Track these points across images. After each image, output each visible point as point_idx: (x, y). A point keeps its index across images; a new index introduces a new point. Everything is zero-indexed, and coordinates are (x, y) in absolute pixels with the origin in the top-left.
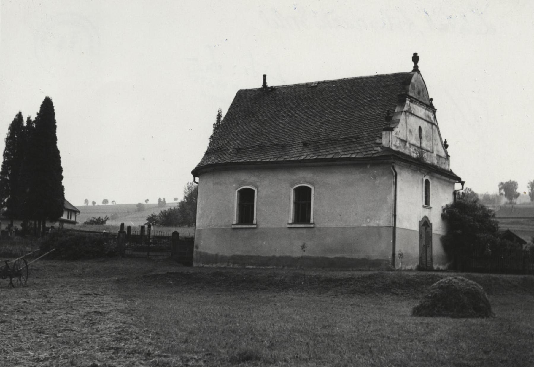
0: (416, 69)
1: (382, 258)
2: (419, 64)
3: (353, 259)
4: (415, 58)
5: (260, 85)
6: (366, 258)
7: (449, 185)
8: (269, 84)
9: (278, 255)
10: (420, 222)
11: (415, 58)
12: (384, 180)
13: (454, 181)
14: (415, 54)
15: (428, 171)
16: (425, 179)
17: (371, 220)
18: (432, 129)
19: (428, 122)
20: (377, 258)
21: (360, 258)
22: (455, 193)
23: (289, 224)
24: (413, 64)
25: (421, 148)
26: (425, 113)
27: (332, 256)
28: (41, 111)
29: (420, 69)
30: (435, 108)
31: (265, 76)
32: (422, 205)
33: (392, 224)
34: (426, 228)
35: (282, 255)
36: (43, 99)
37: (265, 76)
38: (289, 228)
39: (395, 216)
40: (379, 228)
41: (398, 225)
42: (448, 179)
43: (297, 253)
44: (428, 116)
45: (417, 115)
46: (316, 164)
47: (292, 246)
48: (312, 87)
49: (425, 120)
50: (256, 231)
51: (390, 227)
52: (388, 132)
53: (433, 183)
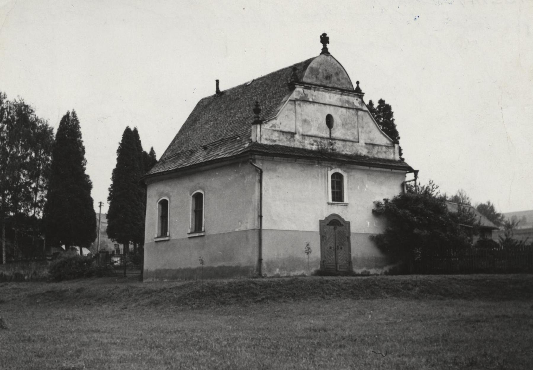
0: (325, 51)
1: (248, 265)
2: (328, 46)
3: (230, 267)
4: (324, 39)
5: (213, 92)
6: (238, 265)
7: (390, 176)
8: (222, 89)
9: (182, 268)
10: (321, 221)
11: (324, 39)
12: (251, 178)
13: (404, 172)
14: (324, 35)
15: (340, 164)
16: (330, 173)
17: (241, 223)
18: (357, 115)
19: (353, 109)
20: (245, 265)
21: (234, 266)
22: (403, 185)
23: (189, 234)
24: (321, 46)
25: (331, 138)
26: (340, 99)
27: (216, 265)
28: (122, 141)
29: (329, 51)
30: (363, 92)
31: (217, 81)
32: (325, 202)
33: (256, 226)
34: (335, 228)
35: (186, 267)
36: (124, 129)
37: (217, 81)
38: (190, 238)
39: (261, 217)
40: (246, 231)
41: (264, 227)
42: (389, 170)
43: (195, 265)
44: (348, 102)
45: (321, 102)
46: (213, 166)
47: (188, 258)
48: (247, 86)
49: (342, 107)
50: (170, 243)
51: (254, 229)
52: (255, 126)
53: (348, 177)
